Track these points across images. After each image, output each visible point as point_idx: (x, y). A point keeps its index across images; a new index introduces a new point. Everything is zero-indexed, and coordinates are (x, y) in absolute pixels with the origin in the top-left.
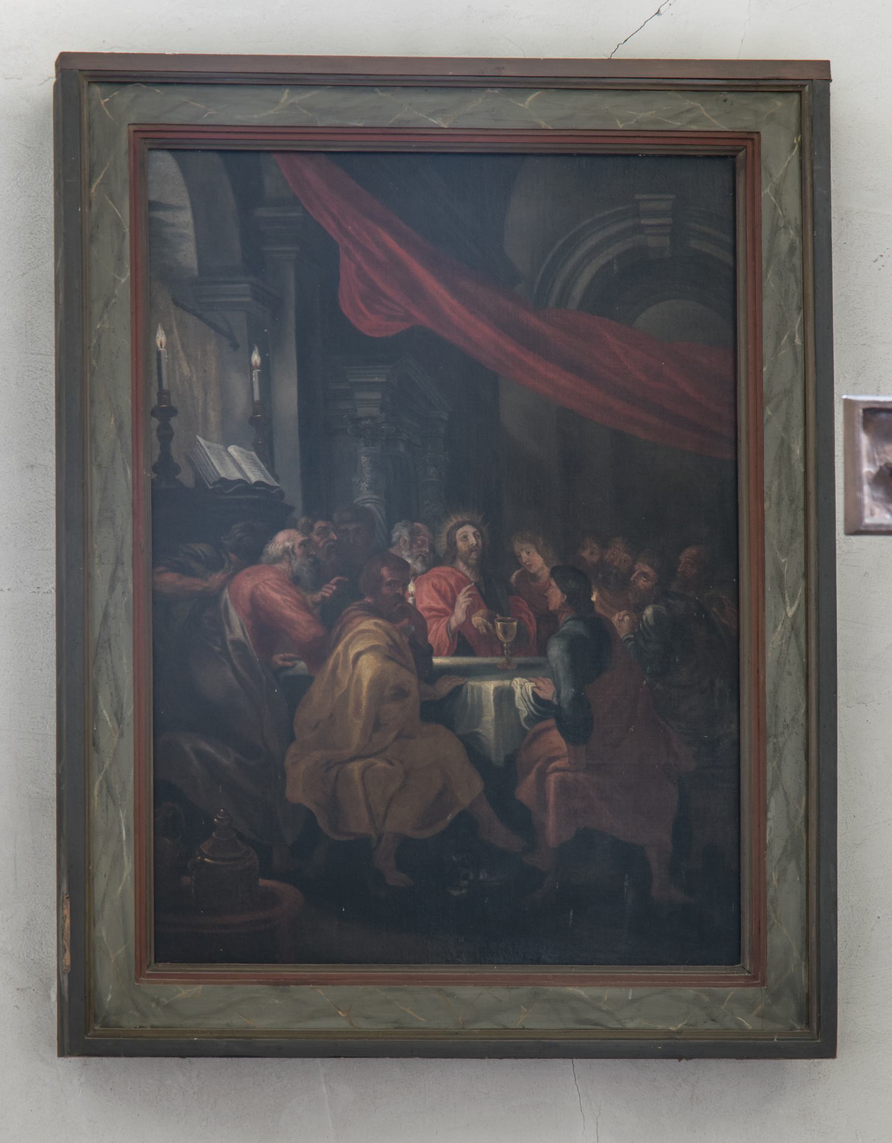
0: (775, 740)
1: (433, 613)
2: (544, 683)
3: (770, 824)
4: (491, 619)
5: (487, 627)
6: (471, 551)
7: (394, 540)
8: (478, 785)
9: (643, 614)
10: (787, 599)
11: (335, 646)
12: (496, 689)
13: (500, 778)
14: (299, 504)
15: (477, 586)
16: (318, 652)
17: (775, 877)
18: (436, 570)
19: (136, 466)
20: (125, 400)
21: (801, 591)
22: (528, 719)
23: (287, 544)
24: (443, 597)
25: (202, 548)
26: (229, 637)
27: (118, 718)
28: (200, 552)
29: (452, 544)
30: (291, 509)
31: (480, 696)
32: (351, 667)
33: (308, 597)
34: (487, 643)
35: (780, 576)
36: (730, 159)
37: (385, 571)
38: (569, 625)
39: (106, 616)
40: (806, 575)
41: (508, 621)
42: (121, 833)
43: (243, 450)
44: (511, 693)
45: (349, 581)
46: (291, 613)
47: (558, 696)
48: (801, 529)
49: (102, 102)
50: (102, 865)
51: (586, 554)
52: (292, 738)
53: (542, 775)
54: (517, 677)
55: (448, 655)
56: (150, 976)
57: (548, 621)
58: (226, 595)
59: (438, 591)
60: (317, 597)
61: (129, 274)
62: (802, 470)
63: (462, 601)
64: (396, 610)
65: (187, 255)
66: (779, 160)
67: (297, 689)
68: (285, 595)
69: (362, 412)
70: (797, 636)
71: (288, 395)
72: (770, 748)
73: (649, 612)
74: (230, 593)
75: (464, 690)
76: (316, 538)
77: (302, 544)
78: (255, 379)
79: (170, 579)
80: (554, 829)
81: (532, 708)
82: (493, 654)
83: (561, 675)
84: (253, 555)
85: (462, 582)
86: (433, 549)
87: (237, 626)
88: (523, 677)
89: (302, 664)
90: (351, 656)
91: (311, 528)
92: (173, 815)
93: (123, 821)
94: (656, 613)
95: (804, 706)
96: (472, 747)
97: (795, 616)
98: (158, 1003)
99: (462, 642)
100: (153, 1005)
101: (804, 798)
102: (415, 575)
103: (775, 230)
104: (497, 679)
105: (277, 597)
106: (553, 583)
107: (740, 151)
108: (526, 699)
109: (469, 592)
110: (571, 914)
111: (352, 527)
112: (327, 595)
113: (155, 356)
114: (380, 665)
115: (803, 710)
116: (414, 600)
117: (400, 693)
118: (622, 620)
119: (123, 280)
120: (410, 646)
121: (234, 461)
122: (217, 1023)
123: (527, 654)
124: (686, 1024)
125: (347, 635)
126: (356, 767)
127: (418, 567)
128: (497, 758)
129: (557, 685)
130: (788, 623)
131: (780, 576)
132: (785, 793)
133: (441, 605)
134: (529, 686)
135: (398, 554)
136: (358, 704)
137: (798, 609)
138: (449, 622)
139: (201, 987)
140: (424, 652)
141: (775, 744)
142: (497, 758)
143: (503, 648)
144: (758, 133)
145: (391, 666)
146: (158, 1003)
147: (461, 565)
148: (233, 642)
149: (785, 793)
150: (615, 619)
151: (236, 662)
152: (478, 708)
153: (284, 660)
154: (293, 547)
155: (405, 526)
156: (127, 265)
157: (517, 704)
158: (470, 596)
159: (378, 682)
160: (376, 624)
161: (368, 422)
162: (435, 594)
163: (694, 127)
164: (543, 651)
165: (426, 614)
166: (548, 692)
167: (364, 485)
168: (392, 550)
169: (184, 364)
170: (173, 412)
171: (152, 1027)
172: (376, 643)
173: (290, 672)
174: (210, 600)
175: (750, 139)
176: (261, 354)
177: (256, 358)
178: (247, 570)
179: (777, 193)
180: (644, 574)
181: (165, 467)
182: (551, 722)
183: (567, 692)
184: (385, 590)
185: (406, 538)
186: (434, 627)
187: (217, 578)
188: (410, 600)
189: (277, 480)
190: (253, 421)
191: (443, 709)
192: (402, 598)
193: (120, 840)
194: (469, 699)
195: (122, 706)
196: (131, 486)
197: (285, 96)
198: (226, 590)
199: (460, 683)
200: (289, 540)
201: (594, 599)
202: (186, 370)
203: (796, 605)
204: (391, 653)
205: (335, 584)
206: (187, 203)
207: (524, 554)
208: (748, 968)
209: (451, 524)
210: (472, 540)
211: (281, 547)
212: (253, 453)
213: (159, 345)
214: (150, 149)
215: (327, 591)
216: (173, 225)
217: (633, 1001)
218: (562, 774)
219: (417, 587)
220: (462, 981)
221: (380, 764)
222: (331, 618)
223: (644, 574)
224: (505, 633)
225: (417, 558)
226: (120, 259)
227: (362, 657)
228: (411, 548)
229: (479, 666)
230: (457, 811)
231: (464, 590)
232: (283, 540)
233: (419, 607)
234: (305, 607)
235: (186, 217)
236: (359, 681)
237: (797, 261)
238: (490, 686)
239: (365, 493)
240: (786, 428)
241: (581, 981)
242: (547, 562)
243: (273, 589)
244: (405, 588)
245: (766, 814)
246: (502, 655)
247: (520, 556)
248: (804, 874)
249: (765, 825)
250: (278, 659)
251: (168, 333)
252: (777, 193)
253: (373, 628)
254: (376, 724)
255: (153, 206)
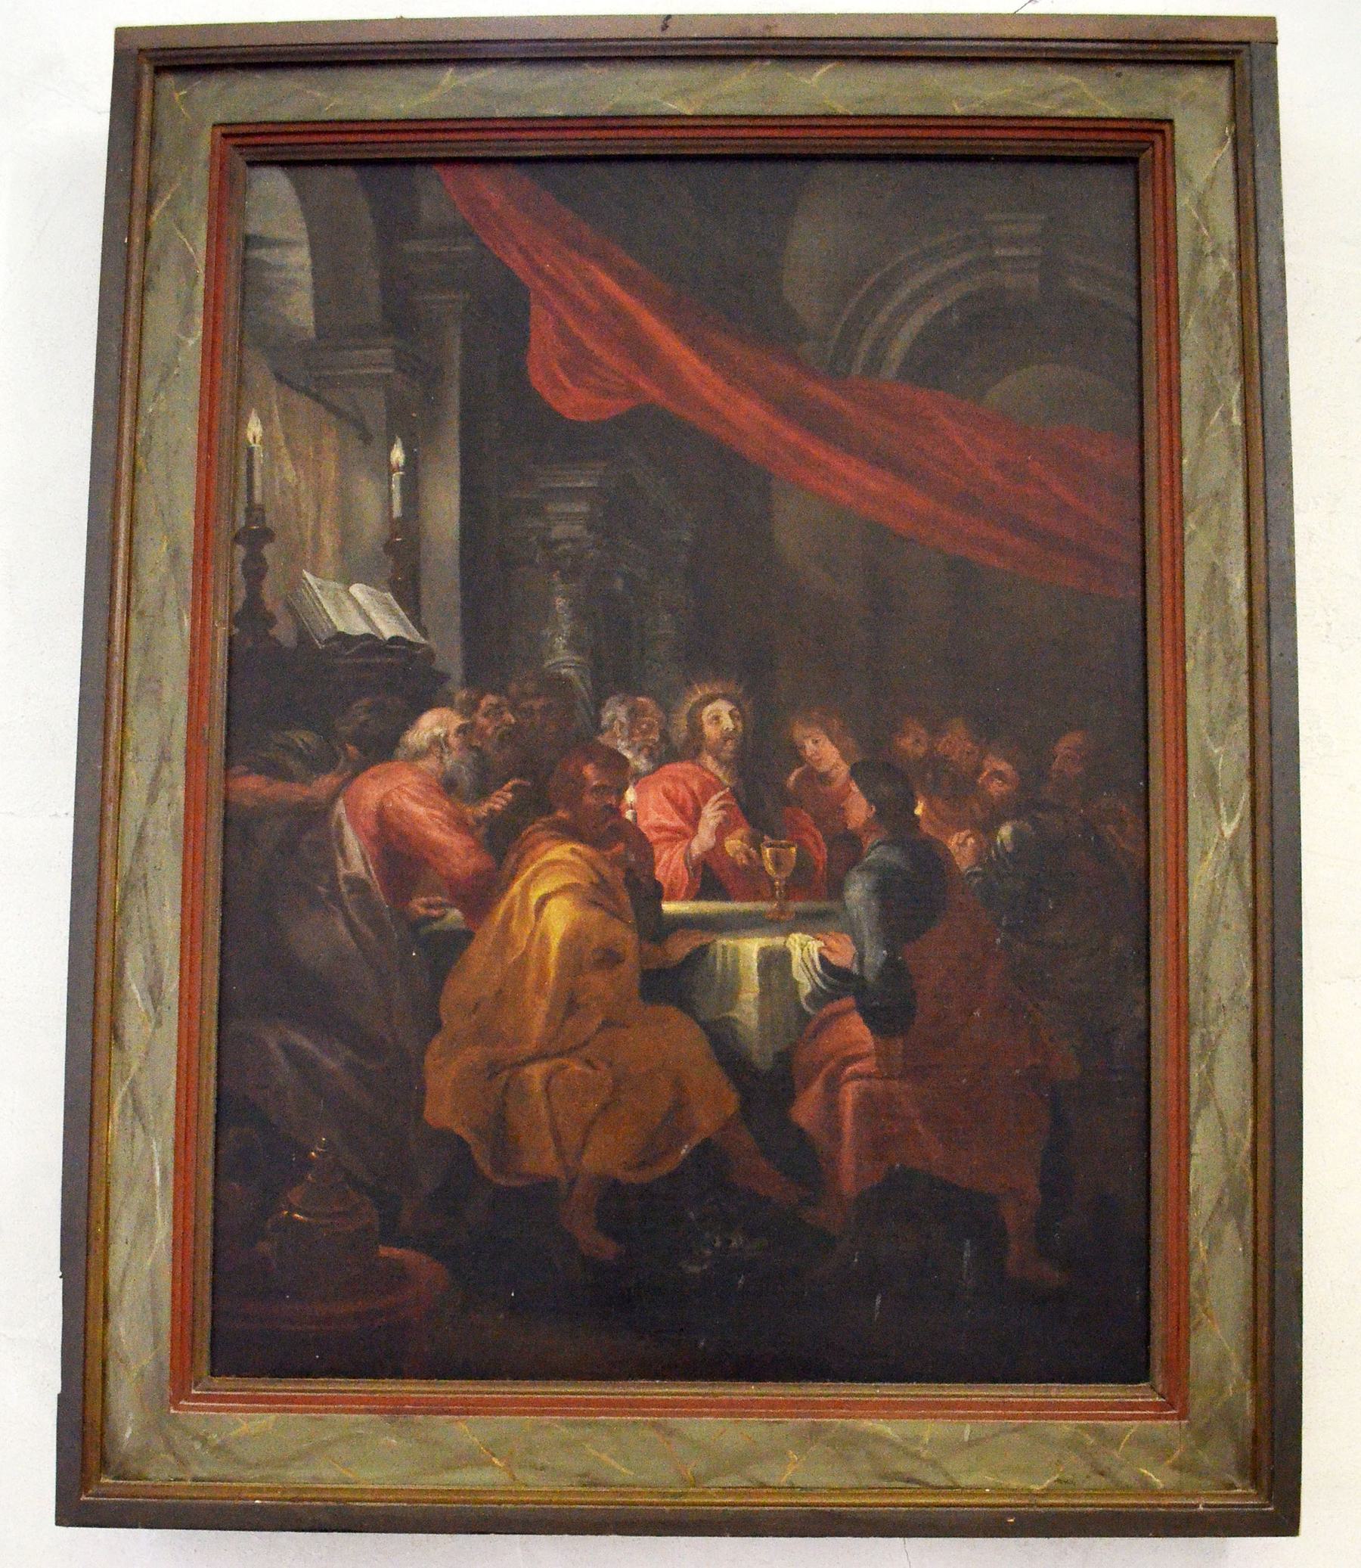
0: (1204, 1031)
1: (664, 834)
2: (837, 941)
3: (1195, 1162)
4: (756, 842)
5: (747, 854)
6: (726, 739)
7: (605, 723)
8: (732, 1103)
9: (996, 834)
10: (1223, 811)
11: (508, 885)
12: (763, 951)
13: (764, 1087)
14: (457, 673)
15: (734, 792)
16: (480, 895)
17: (1203, 1246)
18: (670, 769)
19: (200, 613)
20: (186, 516)
21: (1245, 797)
22: (812, 997)
23: (438, 731)
24: (681, 810)
25: (303, 738)
26: (343, 872)
27: (154, 991)
28: (300, 743)
29: (695, 727)
30: (443, 678)
31: (736, 961)
32: (533, 916)
33: (469, 810)
34: (747, 881)
35: (1211, 775)
36: (1134, 152)
37: (589, 771)
38: (876, 853)
39: (141, 839)
40: (1252, 774)
41: (781, 846)
42: (152, 1174)
43: (371, 589)
44: (785, 956)
45: (539, 784)
46: (440, 835)
47: (861, 962)
48: (1245, 703)
49: (177, 96)
50: (124, 1228)
51: (907, 743)
52: (438, 1026)
53: (833, 1085)
54: (795, 932)
55: (687, 897)
56: (197, 1398)
57: (847, 847)
58: (340, 808)
59: (672, 801)
60: (483, 810)
61: (200, 333)
62: (1245, 612)
63: (711, 815)
64: (606, 831)
65: (299, 309)
66: (1201, 158)
67: (446, 951)
68: (433, 807)
69: (558, 531)
70: (1239, 875)
71: (444, 508)
72: (1195, 1041)
73: (1005, 832)
74: (346, 805)
75: (710, 957)
76: (482, 721)
77: (461, 730)
78: (395, 487)
79: (252, 786)
80: (850, 1170)
81: (818, 980)
82: (756, 896)
83: (866, 928)
84: (382, 747)
85: (709, 787)
86: (665, 737)
87: (356, 856)
88: (805, 932)
89: (455, 914)
90: (533, 901)
91: (475, 706)
92: (240, 1141)
93: (157, 1156)
94: (1016, 834)
95: (1249, 975)
96: (722, 1039)
97: (1235, 835)
98: (204, 1441)
99: (709, 879)
100: (198, 1446)
101: (1250, 1122)
102: (637, 775)
103: (1199, 255)
104: (762, 936)
105: (420, 811)
106: (855, 788)
107: (1144, 150)
108: (810, 965)
109: (722, 803)
110: (878, 1301)
111: (538, 704)
112: (497, 807)
113: (244, 454)
114: (578, 914)
115: (1248, 984)
116: (635, 815)
117: (610, 958)
118: (964, 844)
119: (191, 342)
120: (628, 883)
121: (358, 606)
122: (298, 1475)
123: (811, 895)
124: (1059, 1480)
125: (528, 867)
126: (536, 1072)
127: (641, 763)
128: (762, 1058)
129: (858, 943)
130: (1225, 850)
131: (1211, 775)
132: (1221, 1116)
133: (677, 822)
134: (815, 946)
135: (610, 743)
136: (543, 971)
137: (1240, 825)
138: (689, 847)
139: (272, 1416)
140: (647, 893)
141: (1203, 1035)
142: (762, 1058)
143: (773, 887)
144: (1171, 121)
145: (596, 914)
146: (204, 1441)
147: (709, 762)
148: (348, 879)
149: (1221, 1116)
150: (953, 842)
151: (352, 912)
152: (730, 989)
153: (429, 906)
154: (447, 736)
155: (623, 702)
156: (199, 321)
157: (795, 975)
158: (722, 808)
159: (574, 940)
160: (573, 851)
161: (568, 546)
162: (668, 806)
163: (1071, 112)
164: (836, 889)
165: (653, 836)
166: (844, 955)
167: (560, 641)
168: (603, 739)
169: (288, 465)
170: (268, 535)
171: (195, 1480)
172: (574, 880)
173: (436, 926)
174: (315, 817)
175: (1159, 128)
176: (407, 449)
177: (398, 455)
178: (372, 771)
179: (1201, 205)
180: (998, 774)
181: (251, 616)
182: (848, 1002)
183: (876, 956)
184: (589, 800)
185: (624, 720)
186: (665, 856)
187: (327, 782)
188: (629, 815)
189: (425, 635)
190: (389, 547)
191: (676, 980)
192: (616, 811)
193: (150, 1185)
194: (719, 967)
195: (162, 976)
196: (188, 642)
197: (448, 77)
198: (341, 801)
199: (704, 941)
200: (440, 724)
201: (918, 811)
202: (290, 476)
203: (1237, 819)
204: (596, 894)
205: (513, 790)
206: (304, 236)
207: (809, 745)
208: (1160, 1388)
209: (695, 699)
210: (727, 723)
211: (428, 735)
212: (389, 596)
213: (251, 440)
214: (252, 164)
215: (499, 801)
216: (281, 268)
217: (970, 1444)
218: (864, 1083)
219: (639, 792)
220: (695, 1409)
221: (577, 1068)
222: (503, 843)
223: (1000, 775)
224: (777, 862)
225: (640, 750)
226: (188, 311)
227: (551, 901)
228: (631, 735)
229: (748, 915)
230: (696, 1140)
231: (715, 798)
232: (431, 725)
233: (643, 825)
234: (460, 824)
235: (300, 258)
236: (544, 939)
237: (1233, 304)
238: (751, 947)
239: (562, 657)
240: (1219, 549)
241: (888, 1409)
242: (844, 755)
243: (413, 799)
244: (621, 797)
245: (1188, 1146)
246: (772, 898)
247: (803, 747)
248: (1249, 1237)
249: (1188, 1165)
250: (418, 905)
251: (266, 422)
252: (1201, 205)
253: (570, 857)
254: (570, 1004)
255: (249, 241)
